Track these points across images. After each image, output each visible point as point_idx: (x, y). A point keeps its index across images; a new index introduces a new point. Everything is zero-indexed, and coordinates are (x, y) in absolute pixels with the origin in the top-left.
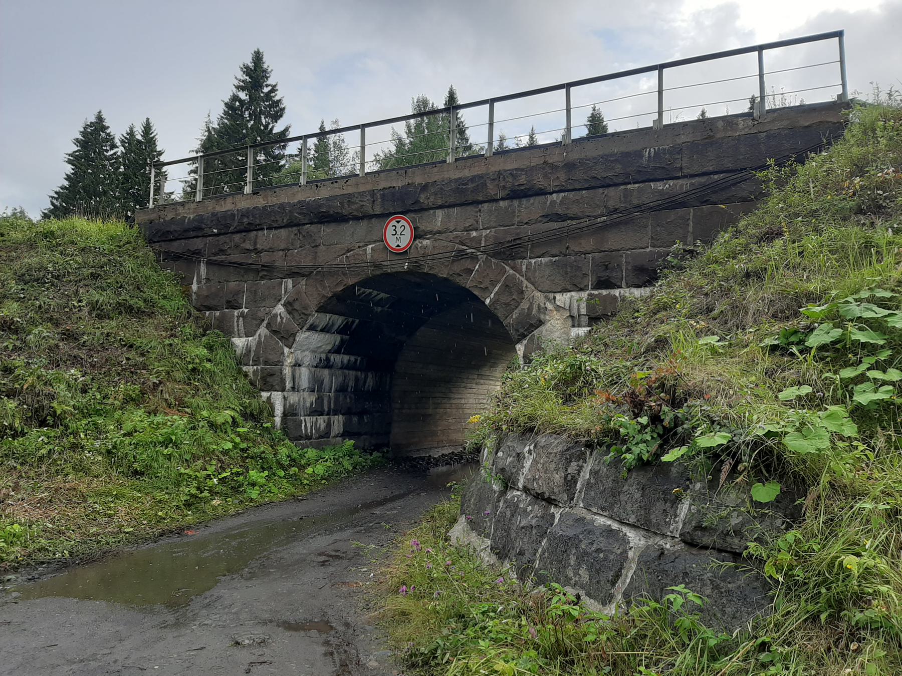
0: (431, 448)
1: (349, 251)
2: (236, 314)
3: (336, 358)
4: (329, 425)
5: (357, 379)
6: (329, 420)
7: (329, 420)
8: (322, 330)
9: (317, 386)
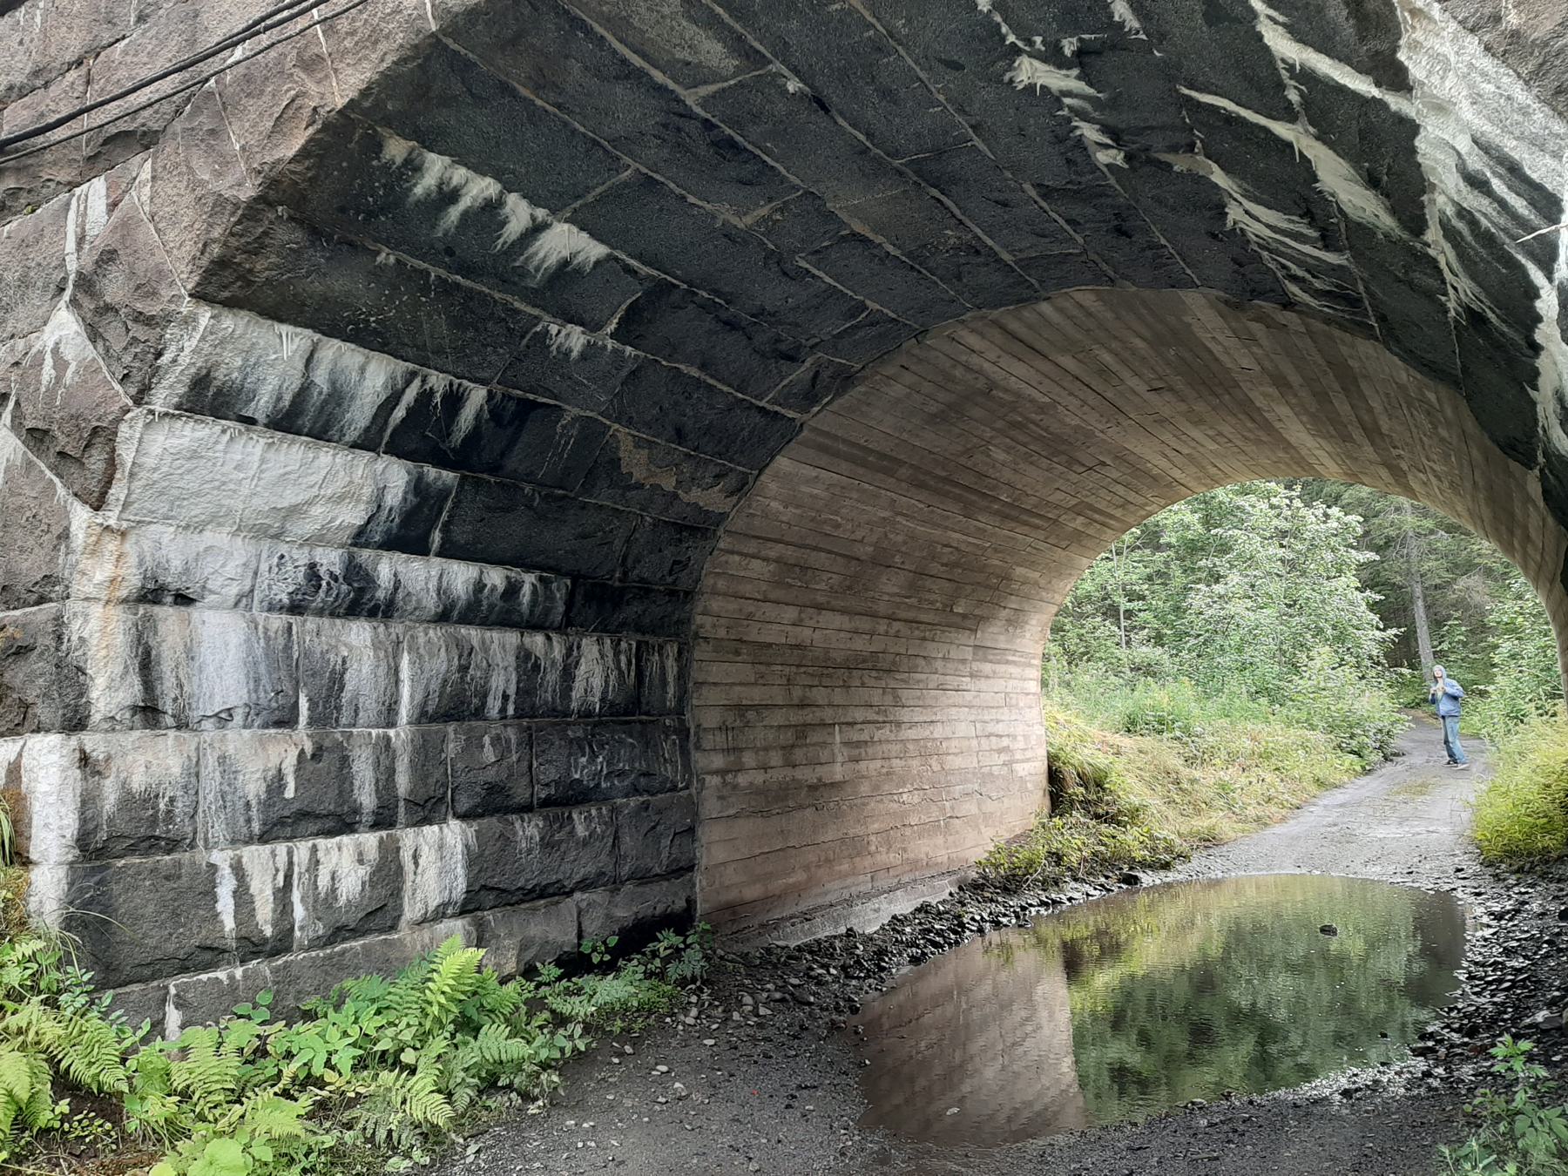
0: (849, 902)
3: (420, 576)
4: (388, 874)
5: (527, 664)
6: (389, 852)
7: (389, 852)
8: (286, 421)
9: (298, 694)
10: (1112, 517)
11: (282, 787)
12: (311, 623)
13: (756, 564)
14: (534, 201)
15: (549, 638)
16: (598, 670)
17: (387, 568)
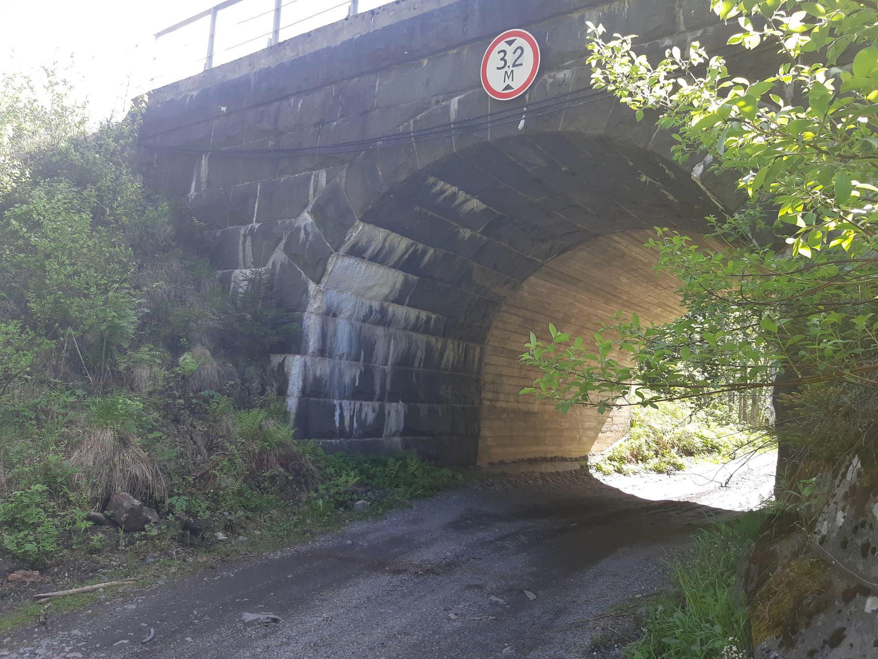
1: (419, 111)
2: (242, 232)
3: (400, 311)
4: (381, 417)
6: (382, 408)
7: (382, 408)
8: (374, 259)
10: (676, 309)
11: (355, 382)
12: (367, 325)
13: (514, 317)
14: (467, 193)
15: (437, 340)
16: (452, 354)
17: (392, 308)
